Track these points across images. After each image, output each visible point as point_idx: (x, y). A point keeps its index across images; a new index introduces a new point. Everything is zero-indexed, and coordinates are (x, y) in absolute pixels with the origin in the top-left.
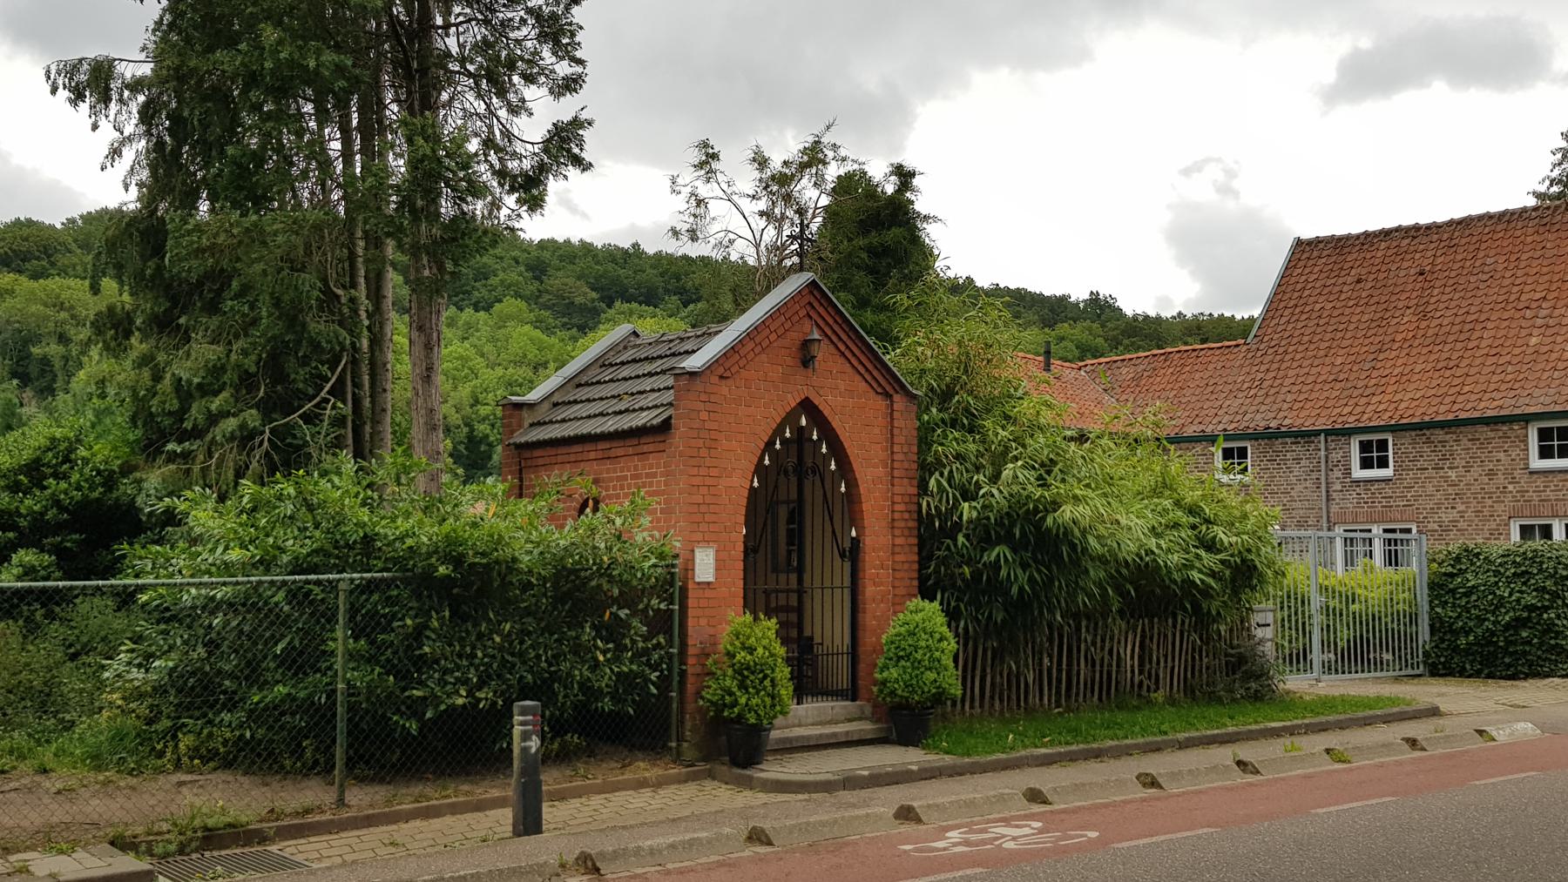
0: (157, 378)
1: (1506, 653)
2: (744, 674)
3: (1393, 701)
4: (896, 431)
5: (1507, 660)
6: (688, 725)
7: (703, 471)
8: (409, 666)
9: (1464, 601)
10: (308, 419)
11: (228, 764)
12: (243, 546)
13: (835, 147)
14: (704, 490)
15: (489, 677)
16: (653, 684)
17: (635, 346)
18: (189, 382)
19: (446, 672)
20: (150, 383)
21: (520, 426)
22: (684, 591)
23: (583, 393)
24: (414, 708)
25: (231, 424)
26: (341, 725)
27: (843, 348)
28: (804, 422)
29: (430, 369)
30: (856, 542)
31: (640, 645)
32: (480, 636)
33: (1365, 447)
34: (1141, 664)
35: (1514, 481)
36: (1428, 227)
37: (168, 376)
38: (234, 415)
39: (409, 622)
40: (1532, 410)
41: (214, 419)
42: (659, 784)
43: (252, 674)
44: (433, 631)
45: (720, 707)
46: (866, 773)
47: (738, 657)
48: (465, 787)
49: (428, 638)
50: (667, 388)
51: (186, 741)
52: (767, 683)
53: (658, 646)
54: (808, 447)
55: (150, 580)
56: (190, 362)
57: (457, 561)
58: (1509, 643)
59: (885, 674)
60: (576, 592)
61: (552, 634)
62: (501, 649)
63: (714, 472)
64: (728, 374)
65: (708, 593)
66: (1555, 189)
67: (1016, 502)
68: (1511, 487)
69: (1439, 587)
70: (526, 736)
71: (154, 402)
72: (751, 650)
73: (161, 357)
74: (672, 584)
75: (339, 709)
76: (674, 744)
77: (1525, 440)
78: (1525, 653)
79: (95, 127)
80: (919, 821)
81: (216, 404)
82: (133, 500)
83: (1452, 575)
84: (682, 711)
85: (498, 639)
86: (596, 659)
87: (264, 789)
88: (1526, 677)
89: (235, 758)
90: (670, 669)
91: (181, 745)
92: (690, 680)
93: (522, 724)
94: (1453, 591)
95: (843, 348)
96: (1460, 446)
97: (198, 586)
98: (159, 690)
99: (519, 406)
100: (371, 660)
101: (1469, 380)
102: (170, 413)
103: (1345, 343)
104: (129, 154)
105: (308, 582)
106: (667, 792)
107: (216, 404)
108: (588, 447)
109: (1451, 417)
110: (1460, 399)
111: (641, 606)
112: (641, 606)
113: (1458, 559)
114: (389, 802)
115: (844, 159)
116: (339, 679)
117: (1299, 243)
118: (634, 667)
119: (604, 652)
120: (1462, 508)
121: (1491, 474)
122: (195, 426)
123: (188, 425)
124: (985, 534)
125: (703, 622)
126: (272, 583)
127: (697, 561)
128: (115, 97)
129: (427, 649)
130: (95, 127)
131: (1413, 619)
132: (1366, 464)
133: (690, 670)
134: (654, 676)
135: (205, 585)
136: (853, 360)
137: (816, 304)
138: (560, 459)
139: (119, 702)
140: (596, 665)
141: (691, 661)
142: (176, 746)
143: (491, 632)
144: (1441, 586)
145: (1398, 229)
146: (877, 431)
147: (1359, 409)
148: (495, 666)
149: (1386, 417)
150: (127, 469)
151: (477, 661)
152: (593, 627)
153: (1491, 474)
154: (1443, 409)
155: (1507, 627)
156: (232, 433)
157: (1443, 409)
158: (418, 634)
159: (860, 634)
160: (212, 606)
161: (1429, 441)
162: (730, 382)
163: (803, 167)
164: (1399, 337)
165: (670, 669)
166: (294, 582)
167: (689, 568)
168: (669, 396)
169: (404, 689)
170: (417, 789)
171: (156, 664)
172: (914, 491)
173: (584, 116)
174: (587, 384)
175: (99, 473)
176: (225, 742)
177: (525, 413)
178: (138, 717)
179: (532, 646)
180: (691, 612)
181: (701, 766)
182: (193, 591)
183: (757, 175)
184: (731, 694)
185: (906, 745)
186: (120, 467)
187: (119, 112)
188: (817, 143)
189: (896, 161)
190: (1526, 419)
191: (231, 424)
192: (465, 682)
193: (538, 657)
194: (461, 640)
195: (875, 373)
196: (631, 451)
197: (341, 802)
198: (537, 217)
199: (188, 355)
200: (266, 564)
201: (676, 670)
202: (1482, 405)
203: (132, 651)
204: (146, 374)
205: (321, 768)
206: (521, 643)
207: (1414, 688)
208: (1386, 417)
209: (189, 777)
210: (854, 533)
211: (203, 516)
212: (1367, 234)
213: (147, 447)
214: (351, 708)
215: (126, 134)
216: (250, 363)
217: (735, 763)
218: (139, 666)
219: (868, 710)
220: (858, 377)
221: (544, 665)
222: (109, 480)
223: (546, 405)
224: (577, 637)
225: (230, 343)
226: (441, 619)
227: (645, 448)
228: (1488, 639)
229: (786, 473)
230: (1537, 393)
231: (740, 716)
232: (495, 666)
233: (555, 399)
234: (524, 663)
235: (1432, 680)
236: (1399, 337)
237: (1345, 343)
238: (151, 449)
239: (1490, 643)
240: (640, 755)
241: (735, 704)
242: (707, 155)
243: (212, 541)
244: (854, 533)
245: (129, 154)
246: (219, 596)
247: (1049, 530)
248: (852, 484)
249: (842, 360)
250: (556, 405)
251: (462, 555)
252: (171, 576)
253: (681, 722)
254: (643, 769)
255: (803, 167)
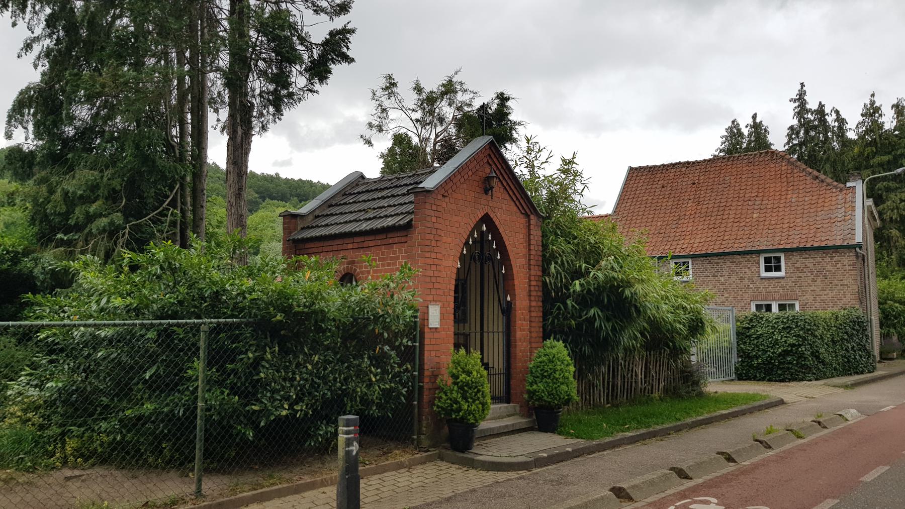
0: (51, 191)
1: (778, 368)
2: (464, 388)
3: (753, 397)
4: (532, 237)
5: (779, 372)
6: (424, 423)
7: (433, 255)
8: (249, 390)
9: (755, 341)
10: (155, 221)
11: (104, 460)
12: (122, 296)
13: (461, 83)
14: (434, 268)
15: (303, 394)
16: (404, 396)
17: (363, 185)
18: (74, 193)
19: (274, 391)
20: (46, 194)
21: (295, 229)
22: (422, 333)
23: (333, 210)
24: (252, 420)
25: (103, 222)
26: (199, 433)
27: (505, 184)
28: (484, 228)
29: (240, 189)
30: (509, 304)
31: (397, 370)
32: (298, 365)
33: (767, 260)
34: (645, 377)
35: (753, 282)
36: (694, 163)
37: (59, 190)
38: (105, 216)
39: (251, 355)
40: (761, 248)
41: (90, 218)
42: (409, 466)
43: (122, 392)
44: (267, 361)
45: (448, 411)
46: (545, 455)
47: (461, 378)
48: (286, 476)
49: (263, 367)
50: (411, 202)
51: (71, 445)
52: (479, 395)
53: (407, 370)
54: (486, 246)
55: (45, 322)
56: (74, 183)
57: (287, 310)
58: (780, 363)
59: (535, 387)
60: (362, 333)
61: (343, 363)
62: (311, 373)
63: (439, 256)
64: (446, 194)
65: (436, 335)
66: (722, 154)
67: (609, 280)
68: (751, 286)
69: (742, 334)
70: (349, 443)
71: (49, 206)
72: (469, 373)
73: (54, 179)
74: (415, 330)
75: (199, 422)
76: (415, 437)
77: (758, 263)
78: (788, 368)
79: (14, 24)
80: (631, 499)
81: (93, 208)
82: (31, 272)
83: (748, 328)
84: (420, 415)
85: (310, 367)
86: (370, 380)
87: (134, 481)
88: (790, 381)
89: (110, 455)
90: (413, 386)
91: (67, 447)
92: (426, 392)
93: (347, 433)
94: (750, 336)
95: (505, 184)
96: (726, 266)
97: (85, 326)
98: (50, 404)
99: (294, 216)
100: (220, 384)
101: (726, 234)
102: (60, 214)
103: (661, 216)
104: (37, 48)
105: (170, 325)
106: (418, 470)
107: (93, 208)
108: (346, 241)
109: (721, 251)
110: (724, 242)
111: (397, 344)
112: (397, 344)
113: (751, 320)
114: (234, 491)
115: (466, 91)
116: (199, 399)
117: (631, 169)
118: (393, 385)
119: (375, 376)
120: (727, 295)
121: (742, 279)
122: (76, 224)
123: (72, 222)
124: (586, 300)
125: (433, 354)
126: (142, 325)
127: (430, 314)
128: (29, 8)
129: (262, 375)
130: (14, 24)
131: (730, 349)
132: (768, 269)
133: (426, 386)
134: (404, 391)
135: (90, 326)
136: (511, 192)
137: (492, 156)
138: (325, 249)
139: (19, 414)
140: (370, 385)
141: (426, 380)
142: (63, 448)
143: (305, 362)
144: (742, 334)
145: (679, 163)
146: (521, 236)
147: (673, 247)
148: (307, 386)
149: (688, 250)
150: (26, 253)
151: (296, 383)
152: (369, 358)
153: (742, 279)
154: (716, 247)
155: (780, 355)
156: (104, 227)
157: (716, 247)
158: (256, 364)
159: (512, 361)
160: (95, 342)
161: (710, 263)
162: (447, 199)
163: (443, 94)
164: (688, 213)
165: (413, 386)
166: (160, 324)
167: (425, 319)
168: (410, 207)
169: (246, 405)
170: (250, 478)
171: (49, 385)
172: (540, 273)
173: (349, 27)
174: (336, 205)
175: (8, 252)
176: (101, 445)
177: (299, 221)
178: (33, 425)
179: (331, 372)
180: (426, 348)
181: (433, 452)
182: (82, 329)
183: (416, 96)
184: (456, 402)
185: (547, 432)
186: (24, 250)
187: (32, 19)
188: (450, 81)
189: (499, 91)
190: (759, 252)
191: (103, 222)
192: (287, 398)
193: (335, 379)
194: (286, 368)
195: (522, 201)
196: (379, 242)
197: (199, 493)
198: (324, 85)
199: (74, 177)
200: (138, 312)
201: (417, 387)
202: (736, 245)
203: (31, 375)
204: (44, 188)
205: (180, 462)
206: (325, 369)
207: (761, 388)
208: (688, 250)
209: (77, 472)
210: (509, 299)
211: (91, 275)
212: (664, 165)
213: (41, 238)
214: (208, 420)
215: (36, 34)
216: (117, 184)
217: (456, 448)
218: (36, 386)
219: (518, 408)
220: (513, 203)
221: (338, 385)
222: (16, 258)
223: (311, 217)
224: (360, 365)
225: (102, 171)
226: (272, 353)
227: (391, 241)
228: (769, 362)
229: (474, 258)
230: (762, 240)
231: (462, 418)
232: (307, 386)
233: (317, 213)
234: (325, 384)
235: (741, 382)
236: (688, 213)
237: (661, 216)
238: (45, 239)
239: (770, 363)
240: (393, 445)
241: (459, 410)
242: (390, 83)
243: (96, 296)
244: (509, 299)
245: (37, 48)
246: (103, 335)
247: (626, 298)
248: (509, 268)
249: (505, 192)
250: (317, 217)
251: (291, 307)
252: (63, 319)
253: (420, 421)
254: (401, 456)
255: (443, 94)
